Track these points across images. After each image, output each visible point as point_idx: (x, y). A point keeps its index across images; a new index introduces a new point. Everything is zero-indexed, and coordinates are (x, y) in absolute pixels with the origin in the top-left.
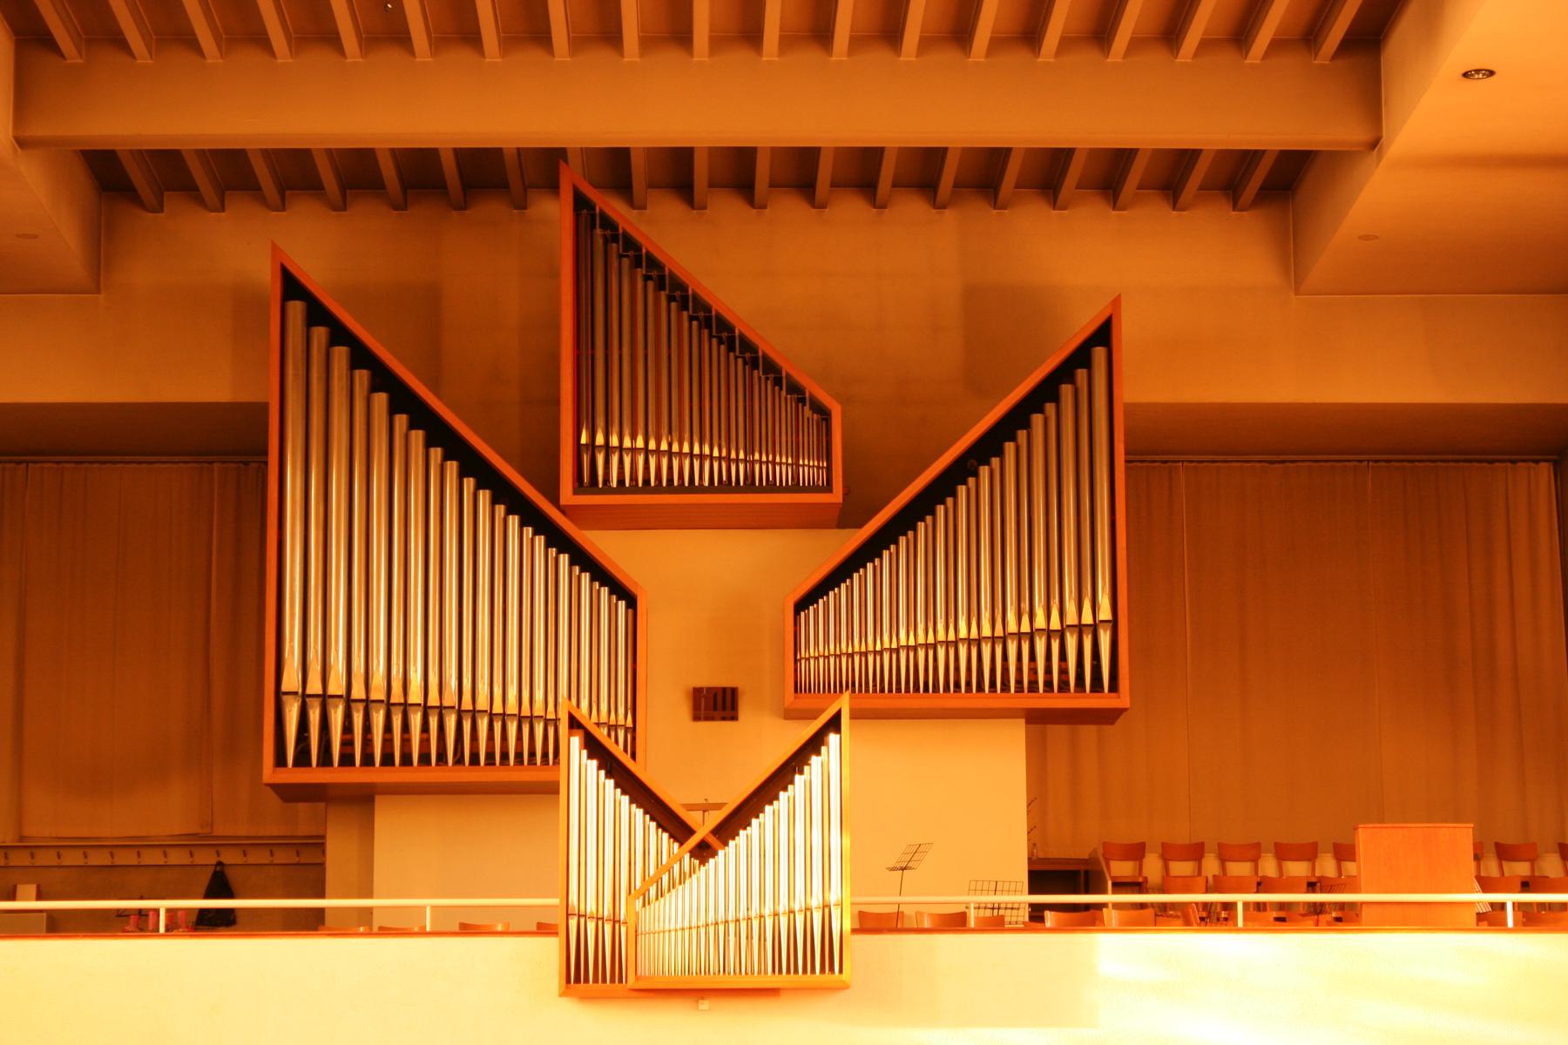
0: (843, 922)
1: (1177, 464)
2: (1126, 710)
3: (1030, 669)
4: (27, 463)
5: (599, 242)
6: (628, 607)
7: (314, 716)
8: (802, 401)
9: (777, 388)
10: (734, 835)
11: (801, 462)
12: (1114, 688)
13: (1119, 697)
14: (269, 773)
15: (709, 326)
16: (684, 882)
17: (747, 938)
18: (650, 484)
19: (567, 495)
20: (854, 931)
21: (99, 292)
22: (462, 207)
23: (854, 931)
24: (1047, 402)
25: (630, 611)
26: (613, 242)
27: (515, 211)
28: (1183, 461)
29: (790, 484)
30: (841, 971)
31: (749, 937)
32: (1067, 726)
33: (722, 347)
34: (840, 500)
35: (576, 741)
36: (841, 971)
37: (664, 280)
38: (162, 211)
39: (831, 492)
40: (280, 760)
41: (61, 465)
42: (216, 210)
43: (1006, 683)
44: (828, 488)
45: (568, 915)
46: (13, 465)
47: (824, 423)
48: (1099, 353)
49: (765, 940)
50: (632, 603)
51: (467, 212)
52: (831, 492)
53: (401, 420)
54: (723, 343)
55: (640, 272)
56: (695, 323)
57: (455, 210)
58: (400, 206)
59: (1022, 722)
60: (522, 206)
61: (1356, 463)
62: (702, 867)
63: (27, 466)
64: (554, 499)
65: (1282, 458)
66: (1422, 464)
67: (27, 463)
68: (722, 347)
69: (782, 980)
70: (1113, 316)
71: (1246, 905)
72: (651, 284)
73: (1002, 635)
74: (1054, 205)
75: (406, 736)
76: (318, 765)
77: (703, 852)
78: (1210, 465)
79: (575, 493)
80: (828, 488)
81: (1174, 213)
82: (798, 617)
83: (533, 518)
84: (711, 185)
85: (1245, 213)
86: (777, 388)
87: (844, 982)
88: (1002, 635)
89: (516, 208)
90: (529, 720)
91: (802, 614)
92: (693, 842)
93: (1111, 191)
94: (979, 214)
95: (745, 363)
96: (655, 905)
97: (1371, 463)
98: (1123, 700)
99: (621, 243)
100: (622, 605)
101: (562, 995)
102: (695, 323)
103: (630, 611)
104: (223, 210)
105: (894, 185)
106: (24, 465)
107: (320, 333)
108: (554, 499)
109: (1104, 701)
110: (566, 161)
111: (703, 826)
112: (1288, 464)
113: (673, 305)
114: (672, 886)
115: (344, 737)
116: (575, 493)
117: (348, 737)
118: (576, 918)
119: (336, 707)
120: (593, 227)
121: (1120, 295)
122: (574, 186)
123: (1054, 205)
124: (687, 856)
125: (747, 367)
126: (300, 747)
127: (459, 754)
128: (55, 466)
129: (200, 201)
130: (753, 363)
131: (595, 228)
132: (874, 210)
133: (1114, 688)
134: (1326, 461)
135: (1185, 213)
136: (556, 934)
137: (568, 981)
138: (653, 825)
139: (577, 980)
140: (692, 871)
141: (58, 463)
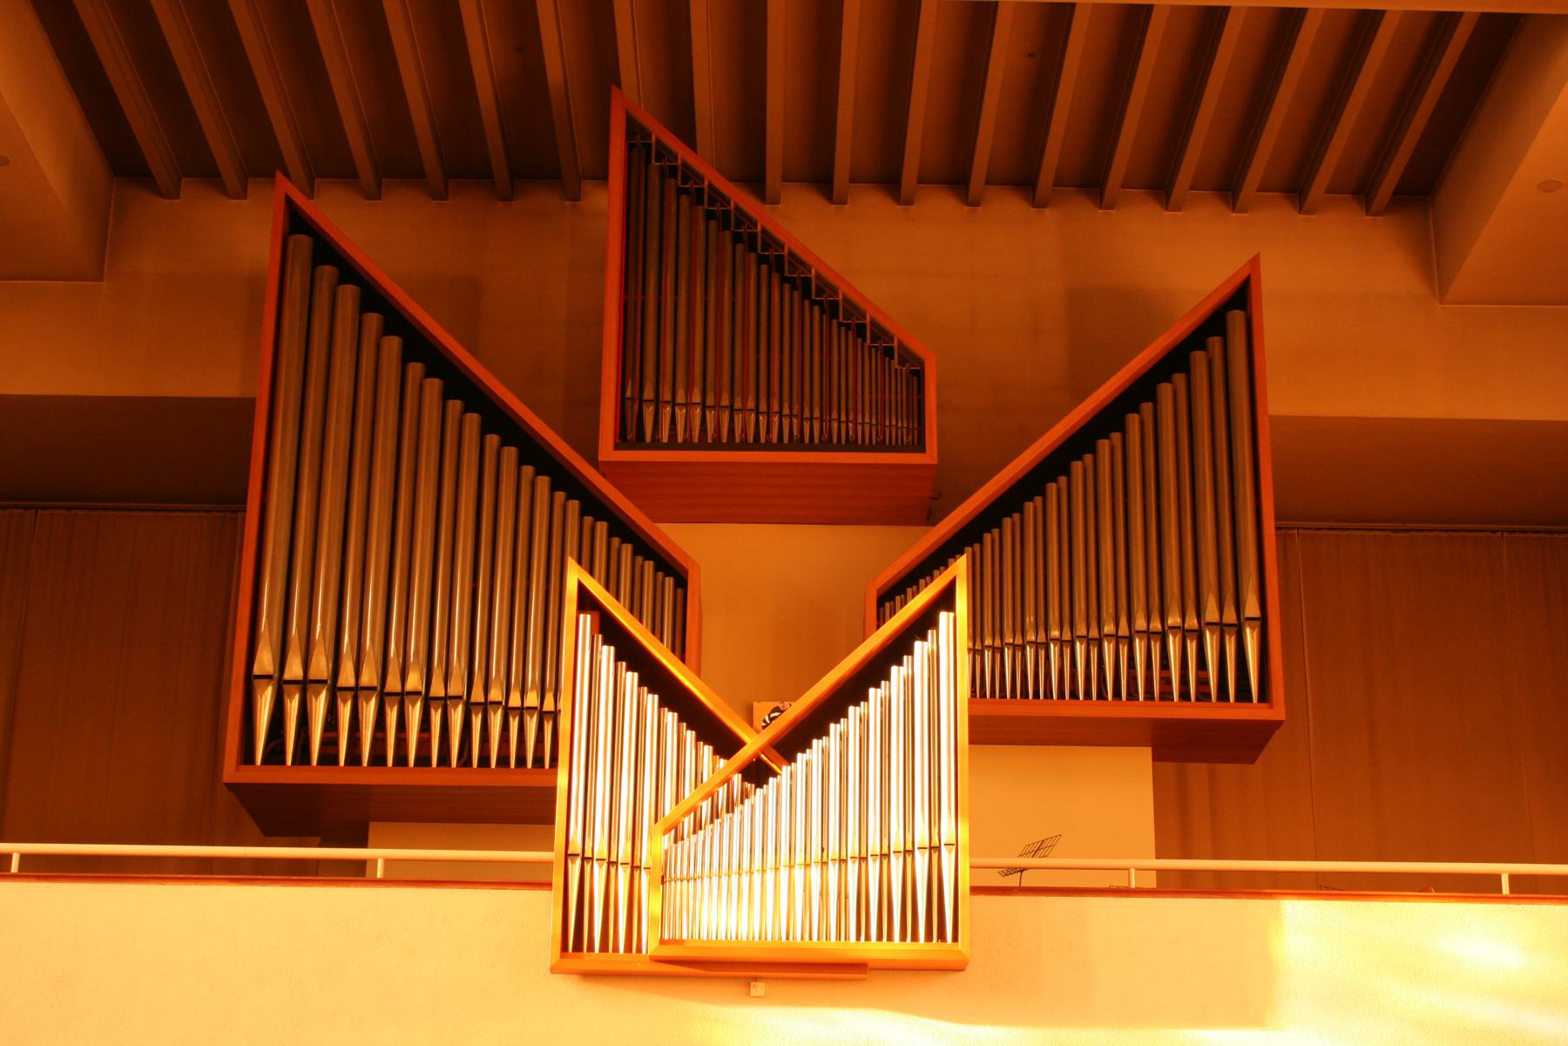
0: (956, 870)
1: (1291, 532)
2: (1281, 722)
3: (1162, 678)
4: (37, 508)
5: (655, 179)
6: (676, 586)
7: (293, 706)
8: (888, 352)
9: (860, 340)
10: (805, 746)
11: (887, 423)
12: (1264, 695)
13: (1271, 707)
14: (231, 771)
15: (780, 269)
16: (733, 812)
17: (821, 894)
18: (707, 440)
19: (607, 450)
20: (975, 890)
21: (102, 280)
22: (507, 197)
23: (975, 890)
24: (1173, 373)
25: (680, 591)
26: (671, 177)
27: (568, 203)
28: (1298, 528)
29: (874, 442)
30: (955, 939)
31: (824, 893)
32: (1205, 764)
33: (796, 293)
34: (935, 461)
35: (586, 620)
36: (955, 939)
37: (729, 216)
38: (178, 197)
39: (924, 451)
40: (247, 756)
41: (73, 512)
42: (237, 197)
43: (1133, 693)
44: (920, 446)
45: (567, 855)
46: (21, 511)
47: (915, 378)
48: (1236, 318)
49: (846, 897)
50: (681, 582)
51: (514, 203)
52: (924, 451)
53: (416, 369)
54: (797, 289)
55: (701, 210)
56: (764, 267)
57: (501, 200)
58: (440, 195)
59: (1142, 758)
60: (575, 197)
61: (1489, 534)
62: (758, 790)
63: (37, 512)
64: (592, 458)
65: (1408, 526)
66: (1561, 536)
67: (37, 508)
68: (796, 293)
69: (874, 949)
70: (1251, 277)
71: (1513, 878)
72: (713, 224)
73: (1127, 634)
74: (1167, 207)
75: (402, 735)
76: (293, 763)
77: (757, 773)
78: (1329, 532)
79: (617, 447)
80: (920, 446)
81: (1302, 216)
82: (882, 609)
83: (565, 481)
84: (785, 179)
85: (1379, 218)
86: (860, 340)
87: (960, 952)
88: (1127, 634)
89: (568, 200)
90: (553, 715)
91: (887, 604)
92: (743, 755)
93: (1230, 193)
94: (1084, 216)
95: (822, 313)
96: (690, 841)
97: (1505, 534)
98: (1275, 712)
99: (679, 178)
100: (669, 581)
101: (554, 970)
102: (764, 267)
103: (680, 591)
104: (245, 197)
105: (987, 183)
106: (33, 511)
107: (327, 272)
108: (592, 458)
109: (1254, 711)
110: (619, 86)
111: (753, 743)
112: (1413, 533)
113: (739, 247)
114: (715, 814)
115: (327, 735)
116: (617, 447)
117: (329, 735)
118: (578, 861)
119: (317, 695)
120: (648, 161)
121: (1259, 254)
122: (627, 113)
123: (1167, 207)
124: (737, 778)
125: (825, 316)
126: (272, 744)
127: (466, 754)
128: (66, 512)
129: (223, 189)
130: (831, 310)
131: (650, 162)
132: (966, 208)
133: (1264, 695)
134: (1457, 531)
135: (1313, 217)
136: (547, 885)
137: (564, 948)
138: (690, 736)
139: (578, 947)
140: (745, 795)
141: (70, 509)
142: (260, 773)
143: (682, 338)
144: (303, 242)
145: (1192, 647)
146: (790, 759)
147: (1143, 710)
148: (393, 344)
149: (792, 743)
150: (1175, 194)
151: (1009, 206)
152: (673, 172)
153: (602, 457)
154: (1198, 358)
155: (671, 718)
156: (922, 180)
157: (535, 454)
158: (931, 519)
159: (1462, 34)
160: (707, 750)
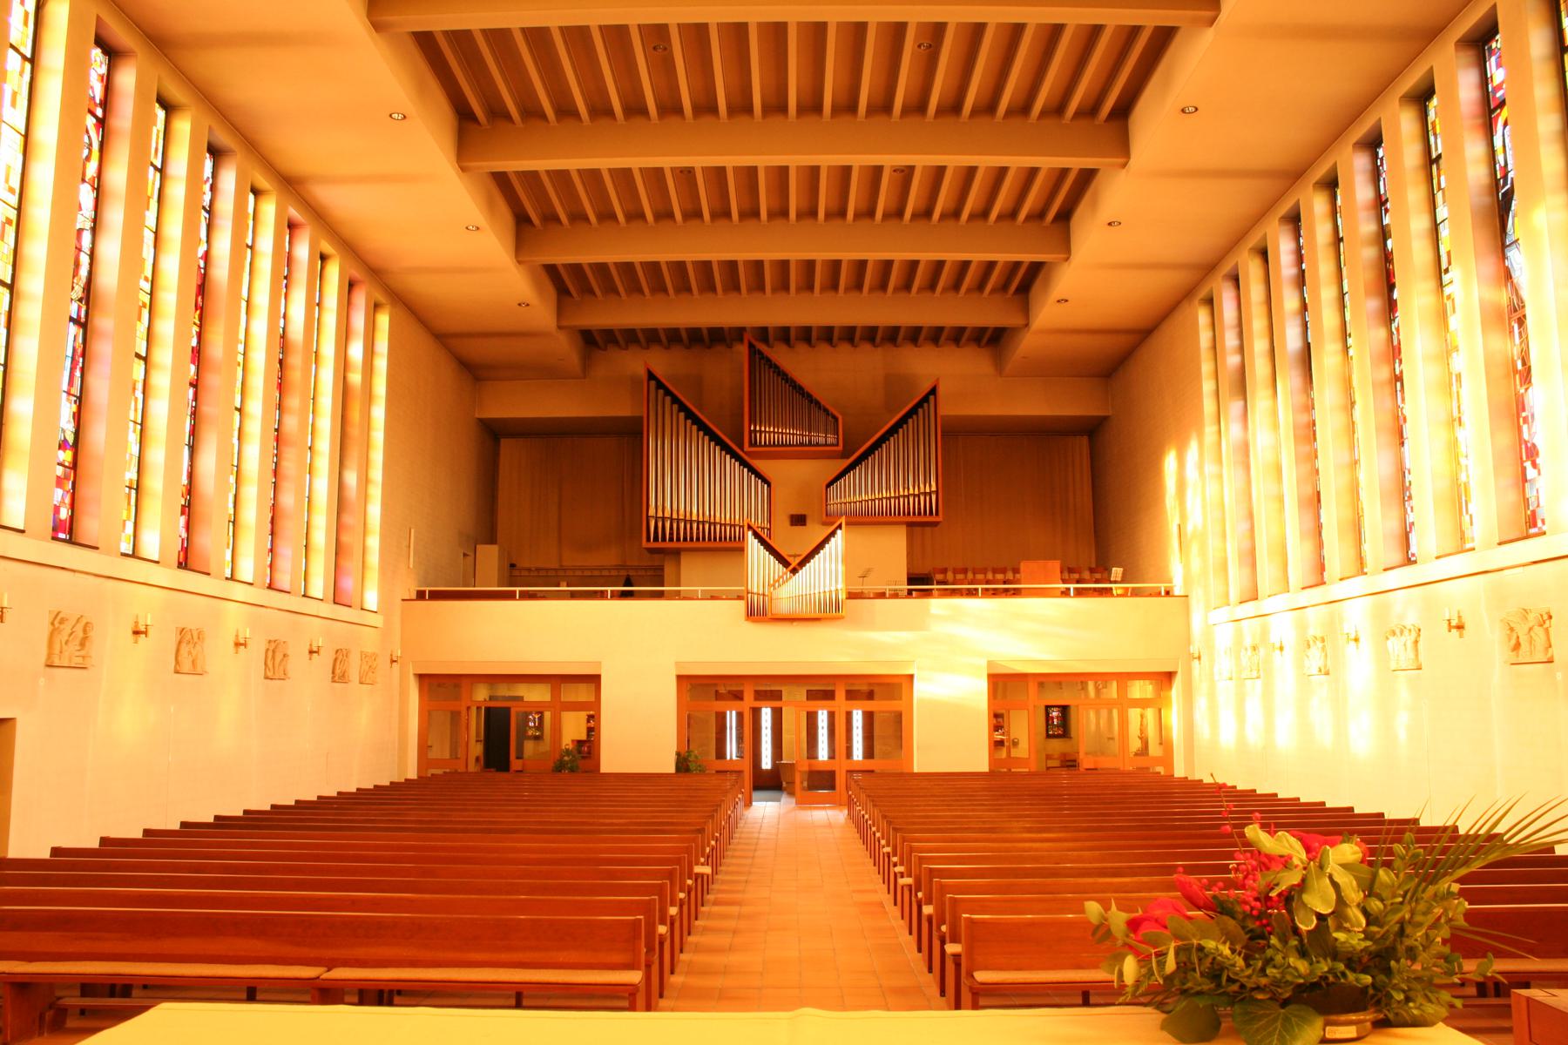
5: (757, 360)
7: (660, 524)
10: (804, 565)
12: (937, 514)
14: (645, 544)
22: (709, 348)
40: (648, 539)
44: (837, 445)
48: (932, 397)
50: (769, 485)
59: (905, 527)
77: (794, 571)
92: (791, 568)
98: (940, 519)
100: (766, 486)
107: (661, 392)
133: (937, 514)
140: (791, 578)
142: (653, 545)
143: (767, 572)
144: (653, 383)
145: (917, 499)
146: (801, 568)
147: (902, 519)
148: (682, 415)
149: (802, 564)
150: (920, 341)
151: (867, 347)
152: (763, 358)
153: (745, 450)
154: (920, 411)
155: (772, 557)
156: (840, 339)
157: (726, 448)
158: (848, 458)
159: (1022, 272)
160: (781, 566)
